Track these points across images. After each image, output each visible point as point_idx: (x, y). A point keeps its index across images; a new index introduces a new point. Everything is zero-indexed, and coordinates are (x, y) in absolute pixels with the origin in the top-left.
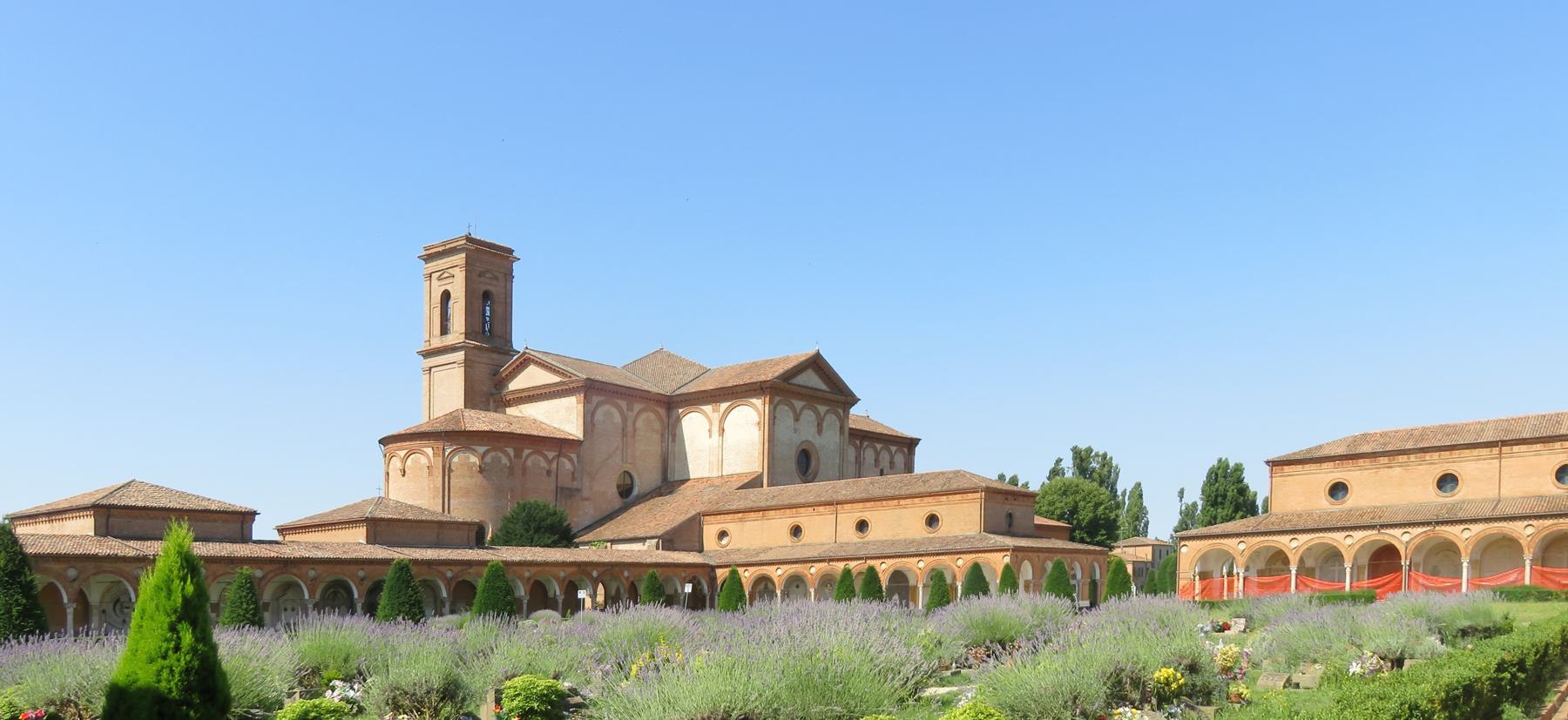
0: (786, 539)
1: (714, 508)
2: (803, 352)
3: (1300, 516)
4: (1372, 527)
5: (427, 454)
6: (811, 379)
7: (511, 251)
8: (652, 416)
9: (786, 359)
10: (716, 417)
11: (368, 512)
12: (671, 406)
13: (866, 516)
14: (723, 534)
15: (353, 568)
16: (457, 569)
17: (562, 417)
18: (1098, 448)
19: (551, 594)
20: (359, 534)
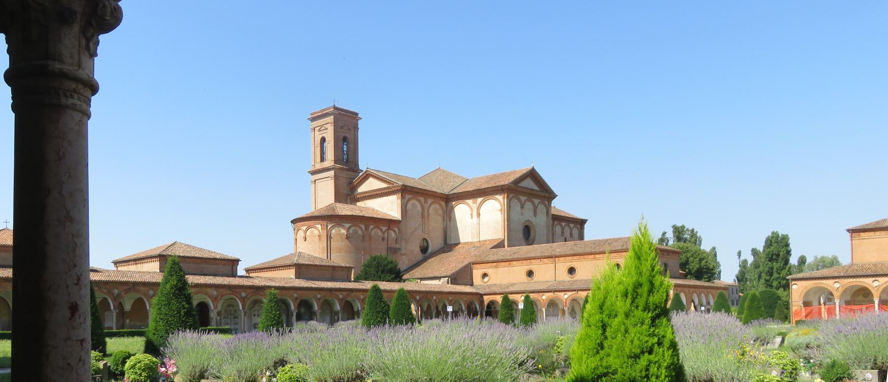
0: (524, 278)
1: (479, 260)
2: (525, 168)
3: (875, 265)
4: (854, 277)
5: (318, 229)
6: (529, 184)
7: (357, 114)
8: (438, 206)
9: (514, 172)
10: (475, 206)
11: (295, 260)
12: (448, 200)
13: (574, 264)
14: (485, 275)
15: (291, 292)
16: (345, 293)
17: (389, 207)
18: (689, 226)
19: (355, 309)
20: (291, 273)
